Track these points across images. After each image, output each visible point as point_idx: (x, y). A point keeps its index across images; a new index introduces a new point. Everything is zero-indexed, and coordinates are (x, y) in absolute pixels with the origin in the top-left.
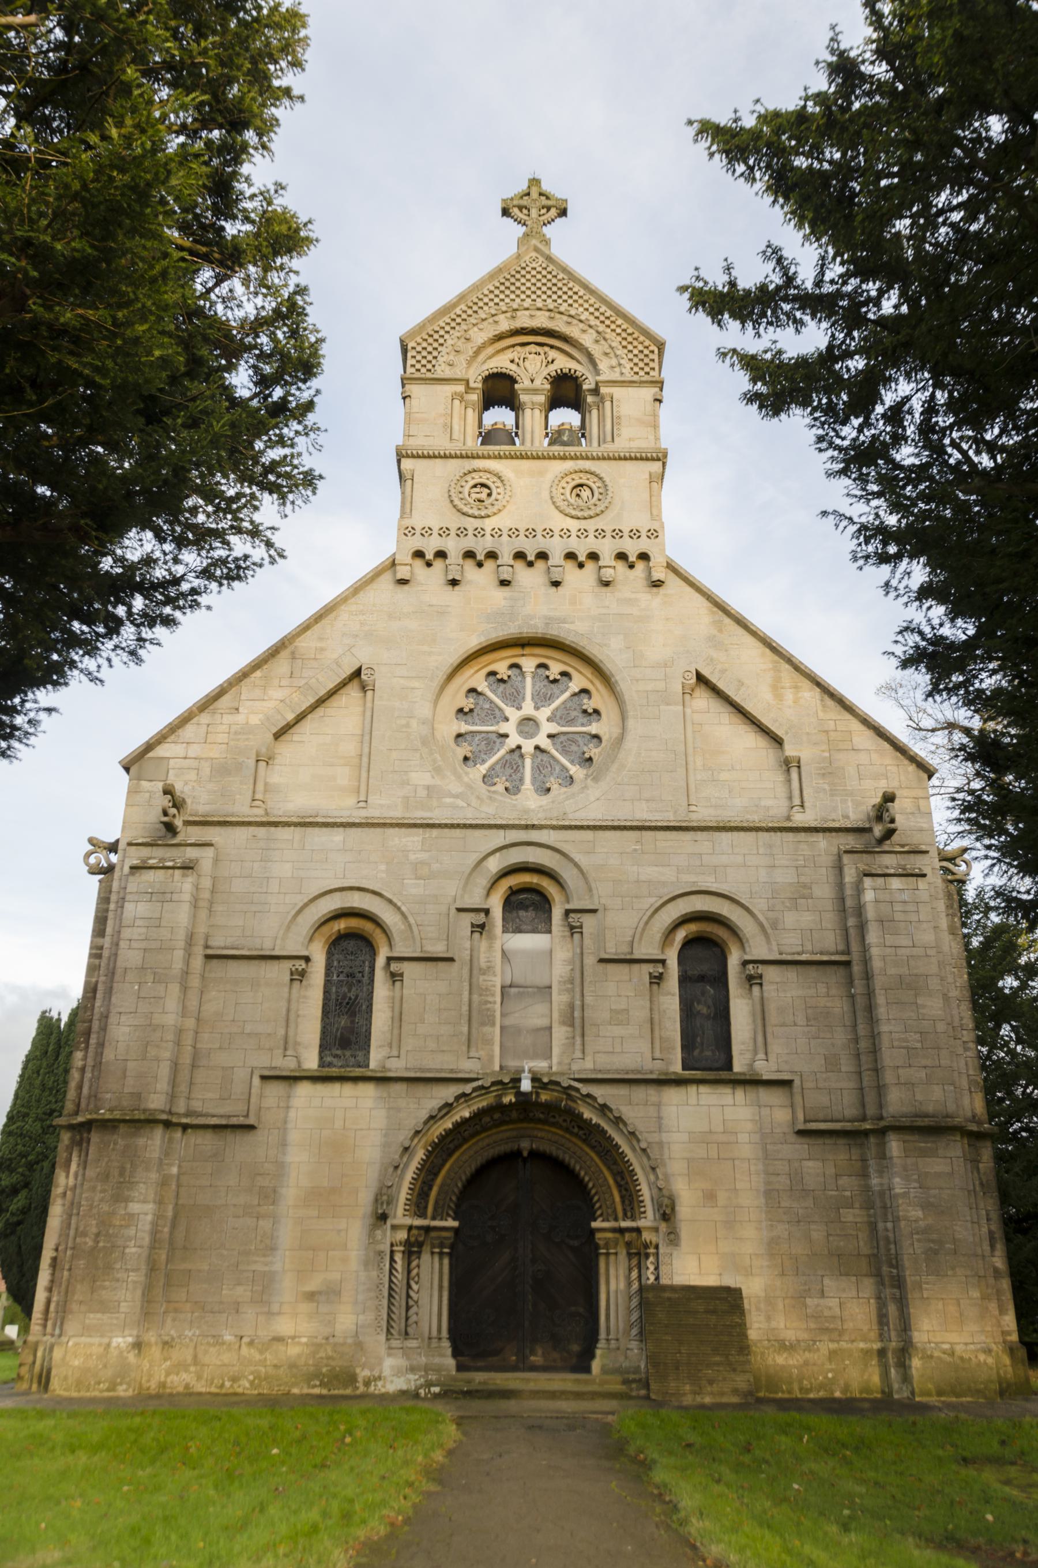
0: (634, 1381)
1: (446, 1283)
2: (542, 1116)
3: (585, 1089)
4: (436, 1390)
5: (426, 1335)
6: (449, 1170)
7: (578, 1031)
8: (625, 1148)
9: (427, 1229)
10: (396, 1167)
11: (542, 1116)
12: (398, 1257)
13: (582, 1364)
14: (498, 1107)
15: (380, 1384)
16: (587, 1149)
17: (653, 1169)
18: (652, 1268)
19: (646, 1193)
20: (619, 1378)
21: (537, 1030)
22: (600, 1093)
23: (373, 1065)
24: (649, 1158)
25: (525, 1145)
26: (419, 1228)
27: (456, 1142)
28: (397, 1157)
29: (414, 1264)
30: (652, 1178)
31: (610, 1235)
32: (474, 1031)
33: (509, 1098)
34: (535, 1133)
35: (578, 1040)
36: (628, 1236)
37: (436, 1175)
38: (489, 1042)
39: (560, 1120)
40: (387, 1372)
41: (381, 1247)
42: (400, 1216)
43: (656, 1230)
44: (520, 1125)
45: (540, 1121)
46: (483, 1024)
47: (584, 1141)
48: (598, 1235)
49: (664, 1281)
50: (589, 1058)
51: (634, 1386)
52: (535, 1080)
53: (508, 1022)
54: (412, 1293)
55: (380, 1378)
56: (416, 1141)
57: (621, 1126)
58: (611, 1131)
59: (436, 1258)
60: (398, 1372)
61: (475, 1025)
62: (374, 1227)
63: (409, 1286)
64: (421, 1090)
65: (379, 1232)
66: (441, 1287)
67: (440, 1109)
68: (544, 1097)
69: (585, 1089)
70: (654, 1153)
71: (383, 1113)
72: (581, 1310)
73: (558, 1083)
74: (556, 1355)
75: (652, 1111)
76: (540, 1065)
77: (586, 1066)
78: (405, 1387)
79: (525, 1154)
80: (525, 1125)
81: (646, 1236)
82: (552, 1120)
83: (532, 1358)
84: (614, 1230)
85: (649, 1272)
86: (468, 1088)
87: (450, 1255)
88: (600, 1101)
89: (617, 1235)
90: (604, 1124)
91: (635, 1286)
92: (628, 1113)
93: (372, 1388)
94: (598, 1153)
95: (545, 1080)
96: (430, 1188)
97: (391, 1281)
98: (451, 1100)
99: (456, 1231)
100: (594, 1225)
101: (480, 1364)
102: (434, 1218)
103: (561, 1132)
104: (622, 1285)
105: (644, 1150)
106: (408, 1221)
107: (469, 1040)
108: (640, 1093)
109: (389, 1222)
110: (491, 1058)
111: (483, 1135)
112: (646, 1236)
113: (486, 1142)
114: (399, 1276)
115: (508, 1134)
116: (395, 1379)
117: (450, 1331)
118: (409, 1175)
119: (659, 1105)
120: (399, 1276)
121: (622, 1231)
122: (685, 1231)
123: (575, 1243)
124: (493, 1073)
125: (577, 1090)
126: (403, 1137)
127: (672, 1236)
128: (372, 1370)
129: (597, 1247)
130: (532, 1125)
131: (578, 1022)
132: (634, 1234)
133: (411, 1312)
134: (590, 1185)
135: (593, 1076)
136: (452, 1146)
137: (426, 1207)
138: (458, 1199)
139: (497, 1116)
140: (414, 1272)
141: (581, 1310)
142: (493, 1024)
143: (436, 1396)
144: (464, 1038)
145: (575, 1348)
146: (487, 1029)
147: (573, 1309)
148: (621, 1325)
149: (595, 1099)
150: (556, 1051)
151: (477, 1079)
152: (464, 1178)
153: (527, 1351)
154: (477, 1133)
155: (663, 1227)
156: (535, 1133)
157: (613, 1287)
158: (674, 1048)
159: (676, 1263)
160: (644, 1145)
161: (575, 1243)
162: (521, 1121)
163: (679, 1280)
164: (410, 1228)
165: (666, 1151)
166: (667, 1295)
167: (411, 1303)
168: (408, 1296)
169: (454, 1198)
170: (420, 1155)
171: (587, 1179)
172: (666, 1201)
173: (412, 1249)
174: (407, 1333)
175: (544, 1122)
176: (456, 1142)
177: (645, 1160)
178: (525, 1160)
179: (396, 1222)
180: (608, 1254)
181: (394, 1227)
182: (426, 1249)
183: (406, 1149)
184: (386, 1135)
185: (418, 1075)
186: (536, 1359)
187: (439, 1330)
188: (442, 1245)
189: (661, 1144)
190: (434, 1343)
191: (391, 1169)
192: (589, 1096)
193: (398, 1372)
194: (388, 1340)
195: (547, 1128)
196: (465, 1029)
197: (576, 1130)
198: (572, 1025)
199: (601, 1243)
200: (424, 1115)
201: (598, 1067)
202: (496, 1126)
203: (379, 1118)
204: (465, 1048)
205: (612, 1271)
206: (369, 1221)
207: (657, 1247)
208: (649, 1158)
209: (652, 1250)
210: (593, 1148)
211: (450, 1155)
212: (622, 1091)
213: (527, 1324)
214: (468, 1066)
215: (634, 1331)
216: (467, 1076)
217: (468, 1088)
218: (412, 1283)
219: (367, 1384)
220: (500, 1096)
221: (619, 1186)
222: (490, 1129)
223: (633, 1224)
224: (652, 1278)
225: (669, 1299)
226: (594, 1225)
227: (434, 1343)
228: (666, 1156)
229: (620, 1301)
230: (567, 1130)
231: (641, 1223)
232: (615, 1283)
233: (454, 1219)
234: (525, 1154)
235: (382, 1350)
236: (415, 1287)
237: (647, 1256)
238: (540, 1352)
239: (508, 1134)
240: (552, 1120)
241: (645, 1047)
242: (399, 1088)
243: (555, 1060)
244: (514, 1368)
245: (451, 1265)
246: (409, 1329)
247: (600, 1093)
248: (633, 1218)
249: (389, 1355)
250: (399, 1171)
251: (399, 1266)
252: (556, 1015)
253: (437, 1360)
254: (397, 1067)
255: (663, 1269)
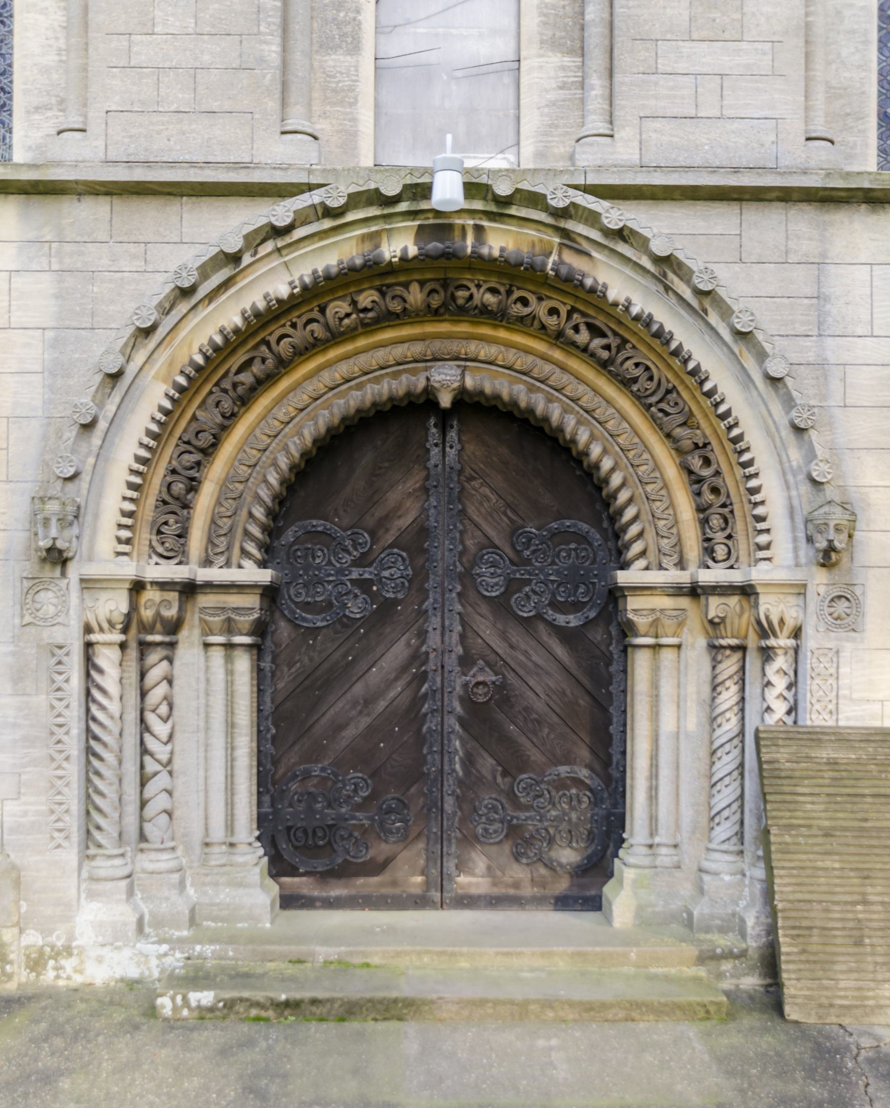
0: (729, 955)
1: (245, 716)
2: (490, 299)
3: (614, 215)
4: (205, 997)
5: (197, 836)
6: (246, 440)
7: (597, 59)
8: (720, 376)
9: (189, 590)
10: (88, 427)
11: (490, 299)
12: (107, 658)
13: (585, 890)
14: (373, 272)
15: (69, 964)
16: (610, 390)
17: (799, 430)
18: (780, 684)
19: (775, 495)
20: (692, 951)
21: (478, 72)
22: (664, 228)
23: (19, 156)
24: (789, 402)
25: (446, 380)
26: (163, 586)
27: (257, 368)
28: (87, 399)
29: (155, 674)
30: (795, 455)
31: (666, 602)
32: (298, 58)
33: (400, 244)
34: (472, 348)
35: (597, 84)
36: (715, 606)
37: (209, 451)
38: (343, 96)
39: (541, 310)
40: (85, 937)
41: (58, 635)
42: (104, 553)
43: (801, 590)
44: (430, 328)
45: (485, 314)
46: (327, 46)
47: (604, 365)
48: (633, 603)
49: (815, 717)
50: (626, 133)
51: (727, 966)
52: (472, 189)
53: (393, 47)
54: (151, 744)
55: (68, 951)
56: (140, 358)
57: (713, 318)
58: (683, 333)
59: (217, 655)
60: (114, 939)
61: (300, 44)
62: (33, 586)
63: (144, 726)
64: (149, 216)
65: (48, 599)
66: (231, 726)
67: (205, 272)
68: (500, 241)
69: (614, 215)
70: (802, 389)
71: (46, 283)
72: (583, 773)
73: (535, 200)
74: (519, 872)
75: (801, 280)
76: (491, 161)
77: (622, 156)
78: (133, 972)
79: (445, 400)
80: (444, 327)
81: (771, 606)
82: (518, 309)
83: (462, 879)
84: (677, 591)
85: (771, 695)
86: (281, 212)
87: (257, 649)
88: (659, 247)
89: (684, 602)
90: (665, 316)
91: (730, 725)
92: (732, 283)
93: (49, 976)
94: (639, 398)
95: (503, 189)
96: (193, 486)
97: (89, 716)
98: (233, 245)
99: (270, 593)
100: (623, 577)
101: (337, 890)
102: (207, 562)
103: (540, 346)
104: (693, 721)
105: (774, 381)
106: (128, 569)
107: (285, 86)
108: (768, 227)
109: (74, 571)
110: (350, 138)
111: (332, 354)
112: (771, 606)
113: (344, 369)
114: (114, 707)
115: (399, 351)
116: (106, 951)
117: (261, 820)
118: (127, 448)
119: (819, 263)
120: (114, 707)
121: (695, 591)
122: (875, 593)
123: (573, 621)
124: (355, 171)
125: (592, 218)
126: (104, 348)
127: (842, 605)
128: (46, 932)
129: (627, 629)
130: (464, 328)
131: (595, 36)
132: (734, 601)
133: (151, 789)
134: (616, 480)
135: (641, 179)
136: (246, 378)
137: (183, 535)
138: (270, 513)
139: (367, 298)
140: (156, 695)
141: (583, 773)
142: (355, 48)
143: (204, 1013)
144: (270, 77)
145: (568, 855)
146: (336, 60)
147: (563, 770)
148: (687, 814)
149: (642, 243)
150: (531, 121)
151: (311, 187)
152: (284, 463)
153: (450, 865)
154: (313, 347)
155: (819, 581)
156: (472, 348)
157: (668, 723)
158: (861, 117)
159: (851, 674)
160: (776, 368)
161: (573, 621)
162: (434, 314)
163: (854, 715)
164: (137, 587)
165: (835, 385)
166: (825, 753)
167: (151, 766)
168: (144, 751)
169: (259, 512)
170: (154, 396)
171: (607, 464)
172: (838, 516)
173: (148, 636)
174: (143, 837)
175: (497, 317)
176: (257, 368)
177: (776, 408)
178: (444, 418)
179: (92, 570)
180: (656, 647)
181: (88, 584)
182: (189, 639)
183: (115, 377)
184: (56, 344)
185: (139, 175)
186: (473, 880)
187: (230, 827)
188: (229, 627)
189: (821, 366)
190: (218, 854)
191: (71, 433)
192: (622, 234)
193: (114, 939)
194: (86, 857)
195: (502, 334)
196: (272, 50)
197: (583, 337)
198: (582, 52)
199: (641, 622)
200: (160, 287)
201: (651, 159)
202: (368, 327)
203: (36, 299)
204: (272, 105)
205: (667, 688)
206: (29, 567)
207: (797, 633)
208: (789, 402)
209: (783, 641)
210: (626, 383)
211: (245, 401)
212: (721, 220)
213: (449, 804)
214: (277, 156)
215: (724, 830)
216: (279, 178)
217: (281, 212)
218: (152, 719)
219: (36, 963)
220: (374, 238)
221: (695, 480)
222: (350, 334)
223: (736, 577)
224: (780, 708)
225: (833, 763)
226: (623, 577)
227: (218, 854)
228: (835, 400)
229: (686, 758)
230: (558, 338)
231: (759, 574)
232: (672, 710)
233: (262, 564)
234: (445, 400)
235: (70, 885)
236: (161, 729)
237: (767, 654)
238: (480, 863)
239: (399, 351)
240: (518, 309)
241: (783, 101)
242: (91, 213)
243: (528, 148)
244: (420, 902)
245: (259, 674)
246: (147, 827)
247: (664, 228)
248: (730, 560)
249: (92, 895)
250: (96, 439)
251: (110, 679)
252: (531, 23)
253: (225, 895)
254: (80, 159)
255: (811, 689)
